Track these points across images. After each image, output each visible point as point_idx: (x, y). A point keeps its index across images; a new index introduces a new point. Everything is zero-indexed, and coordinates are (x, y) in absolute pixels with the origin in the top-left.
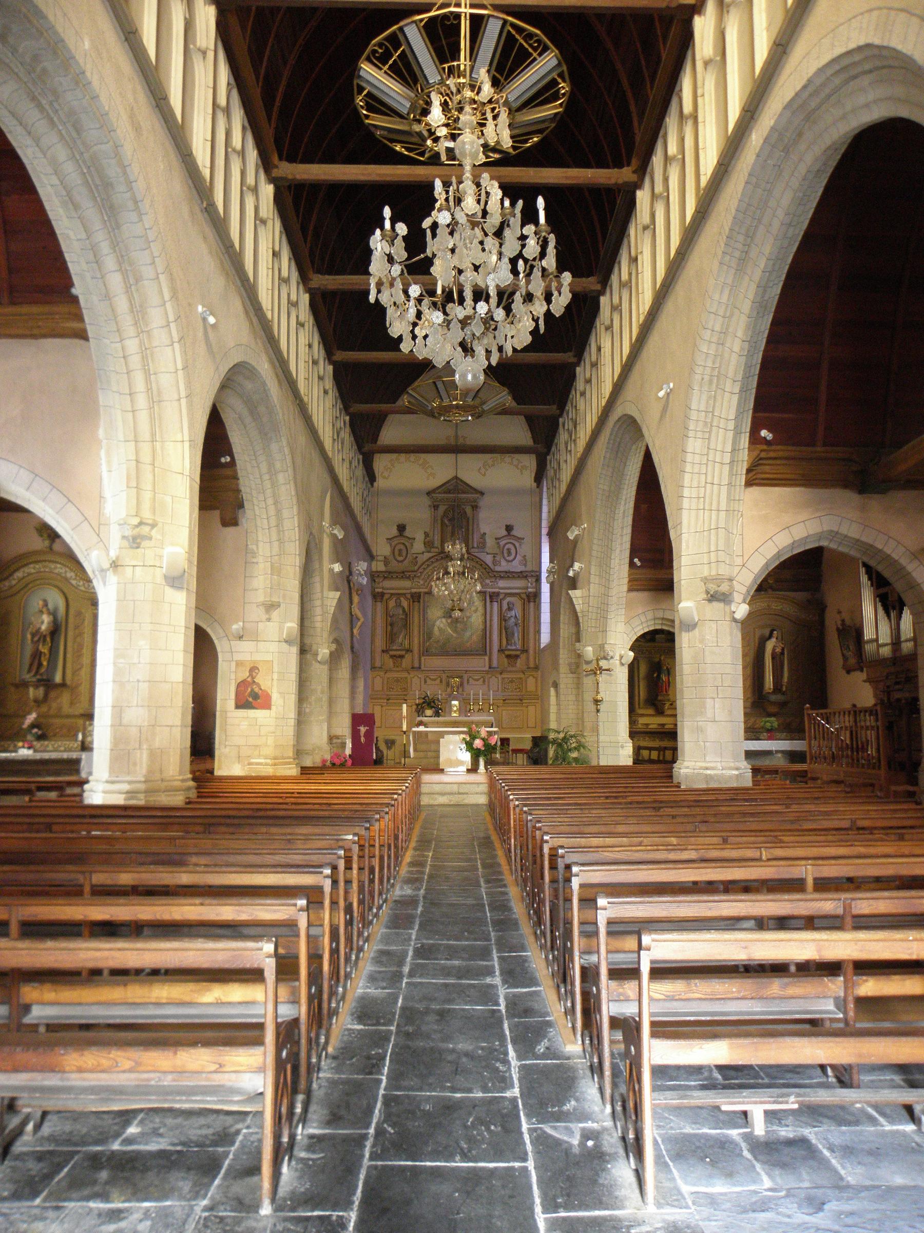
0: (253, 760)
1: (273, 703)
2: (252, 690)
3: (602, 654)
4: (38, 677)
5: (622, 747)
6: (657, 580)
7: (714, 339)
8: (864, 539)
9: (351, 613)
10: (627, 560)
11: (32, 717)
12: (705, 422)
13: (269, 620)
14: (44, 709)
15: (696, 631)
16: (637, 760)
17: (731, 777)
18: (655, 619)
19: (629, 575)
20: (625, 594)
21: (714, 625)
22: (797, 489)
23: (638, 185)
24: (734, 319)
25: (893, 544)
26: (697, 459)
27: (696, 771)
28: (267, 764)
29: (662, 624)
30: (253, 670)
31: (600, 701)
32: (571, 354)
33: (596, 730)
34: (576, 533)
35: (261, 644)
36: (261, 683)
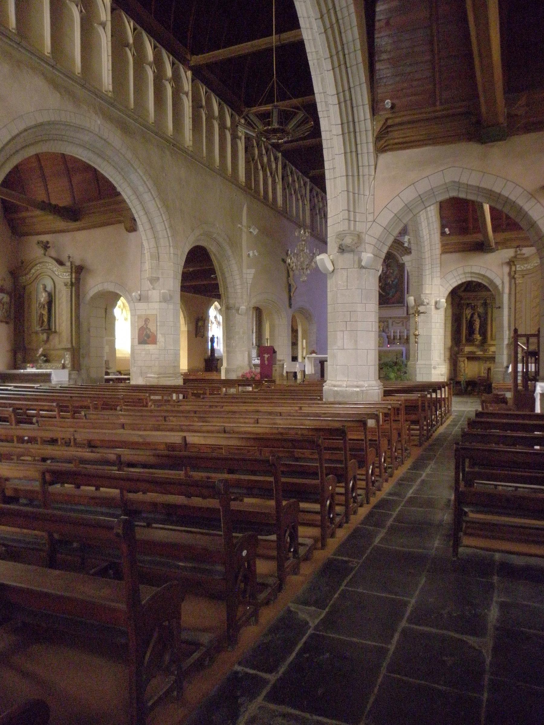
0: (149, 375)
1: (158, 340)
2: (147, 332)
4: (43, 328)
5: (435, 368)
9: (288, 282)
11: (41, 350)
13: (154, 289)
14: (47, 346)
17: (353, 393)
19: (441, 242)
21: (345, 273)
28: (154, 378)
30: (147, 320)
31: (418, 335)
35: (150, 304)
36: (151, 329)
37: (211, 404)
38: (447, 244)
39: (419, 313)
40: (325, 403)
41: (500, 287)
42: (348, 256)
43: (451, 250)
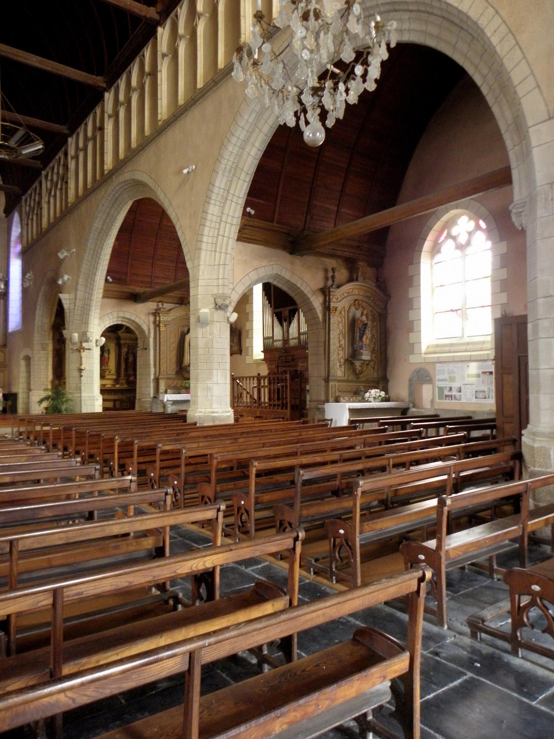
3: (85, 338)
6: (122, 292)
7: (238, 144)
8: (292, 281)
10: (104, 278)
12: (223, 196)
15: (208, 328)
16: (105, 409)
18: (118, 317)
19: (105, 287)
20: (100, 299)
22: (261, 247)
23: (160, 23)
24: (255, 135)
25: (305, 285)
26: (214, 219)
27: (206, 414)
29: (122, 321)
32: (65, 127)
33: (79, 389)
34: (65, 254)
37: (179, 432)
38: (108, 291)
39: (84, 349)
40: (241, 424)
41: (147, 332)
42: (221, 312)
43: (110, 296)
